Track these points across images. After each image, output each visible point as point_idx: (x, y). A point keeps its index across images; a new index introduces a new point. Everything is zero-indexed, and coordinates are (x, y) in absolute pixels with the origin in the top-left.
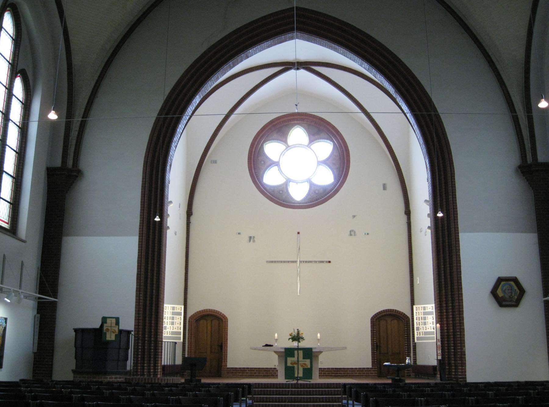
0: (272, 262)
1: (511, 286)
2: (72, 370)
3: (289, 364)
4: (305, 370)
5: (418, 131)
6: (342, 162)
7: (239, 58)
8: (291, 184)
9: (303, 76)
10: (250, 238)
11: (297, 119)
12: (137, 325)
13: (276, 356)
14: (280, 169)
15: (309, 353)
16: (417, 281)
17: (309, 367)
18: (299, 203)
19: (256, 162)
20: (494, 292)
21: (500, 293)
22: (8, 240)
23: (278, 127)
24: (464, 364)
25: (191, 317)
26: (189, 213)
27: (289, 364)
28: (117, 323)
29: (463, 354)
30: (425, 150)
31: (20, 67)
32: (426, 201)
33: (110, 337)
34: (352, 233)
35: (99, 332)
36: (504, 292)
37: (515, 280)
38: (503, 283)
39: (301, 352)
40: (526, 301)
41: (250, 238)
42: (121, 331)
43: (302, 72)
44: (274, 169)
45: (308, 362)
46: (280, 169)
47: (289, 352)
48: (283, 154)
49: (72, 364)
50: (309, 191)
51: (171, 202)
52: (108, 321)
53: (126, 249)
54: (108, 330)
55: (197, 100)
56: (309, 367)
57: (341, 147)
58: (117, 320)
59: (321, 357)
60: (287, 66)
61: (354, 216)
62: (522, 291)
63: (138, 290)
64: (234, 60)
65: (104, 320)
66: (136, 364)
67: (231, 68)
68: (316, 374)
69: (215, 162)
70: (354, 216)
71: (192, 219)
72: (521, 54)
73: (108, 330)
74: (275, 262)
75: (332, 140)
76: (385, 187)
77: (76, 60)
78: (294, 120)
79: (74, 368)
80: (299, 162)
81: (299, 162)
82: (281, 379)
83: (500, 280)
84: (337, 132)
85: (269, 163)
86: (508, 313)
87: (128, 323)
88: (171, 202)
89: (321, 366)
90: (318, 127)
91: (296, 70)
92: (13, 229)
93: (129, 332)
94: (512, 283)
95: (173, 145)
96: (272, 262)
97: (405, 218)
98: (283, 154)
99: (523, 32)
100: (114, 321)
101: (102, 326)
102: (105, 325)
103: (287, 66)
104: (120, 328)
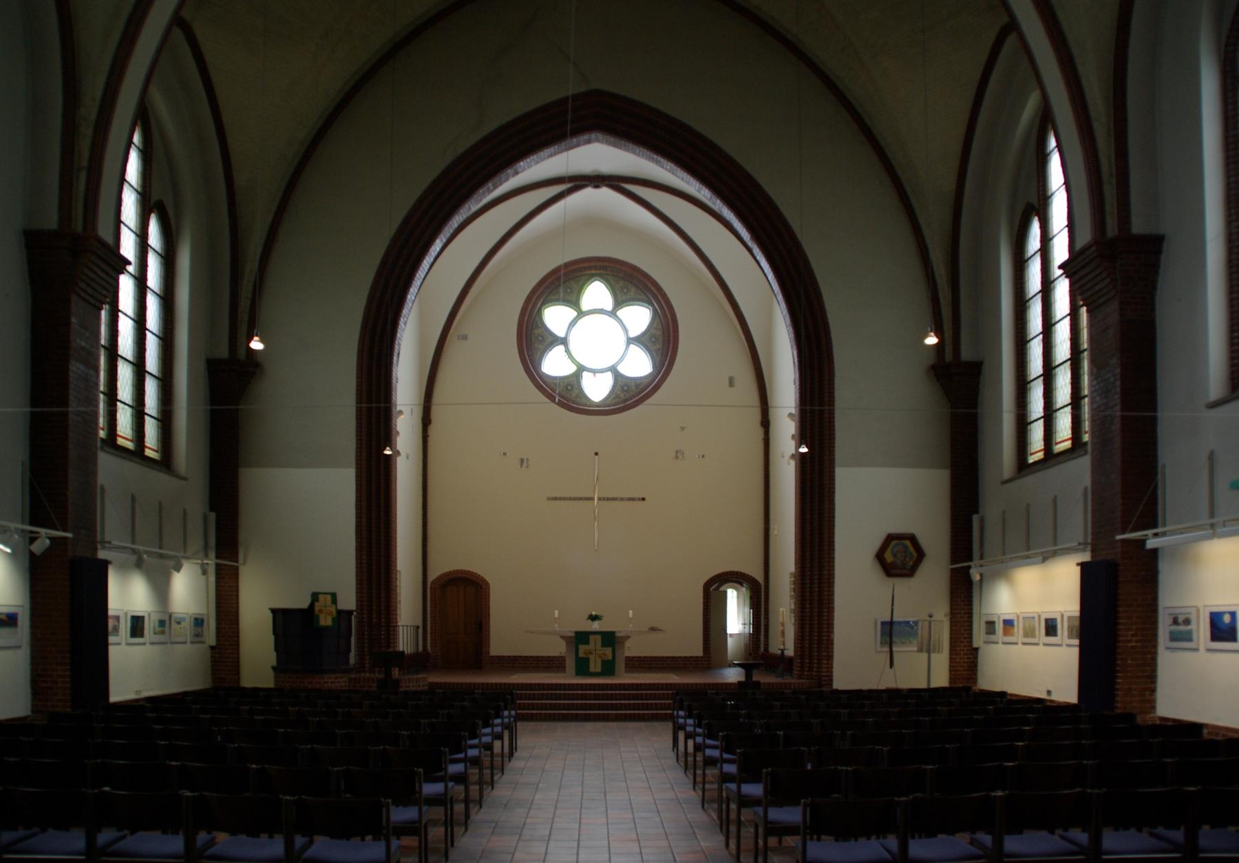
0: (556, 499)
1: (905, 547)
2: (273, 668)
3: (581, 655)
4: (604, 663)
5: (783, 305)
6: (663, 340)
7: (503, 176)
8: (585, 374)
9: (606, 196)
10: (522, 460)
11: (596, 268)
12: (360, 600)
13: (563, 643)
14: (567, 351)
15: (610, 639)
16: (774, 531)
17: (610, 658)
18: (597, 405)
19: (532, 339)
20: (880, 556)
21: (889, 557)
22: (162, 477)
23: (563, 282)
24: (830, 657)
25: (434, 582)
26: (426, 421)
27: (581, 655)
28: (334, 601)
29: (830, 643)
30: (792, 335)
31: (155, 198)
32: (790, 415)
33: (326, 621)
34: (678, 454)
35: (308, 614)
36: (895, 555)
37: (912, 538)
38: (894, 543)
39: (599, 637)
40: (925, 569)
41: (522, 460)
42: (340, 612)
43: (605, 193)
44: (559, 350)
45: (608, 651)
46: (567, 351)
47: (582, 637)
48: (573, 323)
49: (271, 658)
50: (614, 386)
51: (401, 412)
52: (321, 597)
53: (334, 489)
54: (321, 611)
55: (438, 245)
56: (610, 658)
57: (665, 315)
58: (334, 595)
59: (627, 644)
60: (579, 182)
61: (683, 428)
62: (921, 555)
63: (359, 550)
64: (496, 180)
65: (315, 597)
66: (361, 655)
67: (490, 191)
68: (620, 665)
69: (465, 337)
70: (683, 428)
71: (432, 430)
72: (948, 183)
73: (321, 611)
74: (561, 499)
75: (650, 303)
76: (731, 383)
77: (241, 179)
78: (590, 268)
79: (274, 663)
80: (599, 341)
81: (599, 341)
82: (568, 678)
83: (890, 538)
84: (660, 289)
85: (548, 341)
86: (901, 585)
87: (348, 600)
88: (401, 412)
89: (628, 654)
90: (630, 282)
91: (594, 187)
92: (166, 462)
93: (350, 613)
94: (907, 543)
95: (402, 320)
96: (556, 499)
97: (760, 432)
98: (573, 323)
99: (957, 148)
100: (329, 598)
101: (312, 605)
102: (317, 605)
103: (579, 182)
104: (340, 607)
